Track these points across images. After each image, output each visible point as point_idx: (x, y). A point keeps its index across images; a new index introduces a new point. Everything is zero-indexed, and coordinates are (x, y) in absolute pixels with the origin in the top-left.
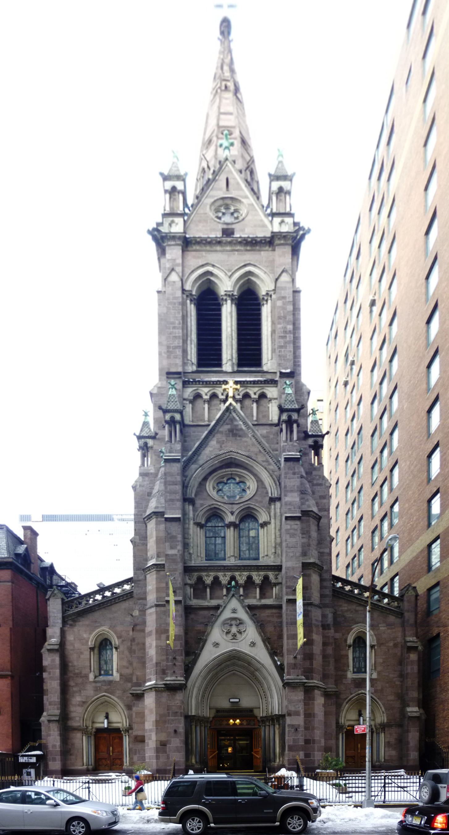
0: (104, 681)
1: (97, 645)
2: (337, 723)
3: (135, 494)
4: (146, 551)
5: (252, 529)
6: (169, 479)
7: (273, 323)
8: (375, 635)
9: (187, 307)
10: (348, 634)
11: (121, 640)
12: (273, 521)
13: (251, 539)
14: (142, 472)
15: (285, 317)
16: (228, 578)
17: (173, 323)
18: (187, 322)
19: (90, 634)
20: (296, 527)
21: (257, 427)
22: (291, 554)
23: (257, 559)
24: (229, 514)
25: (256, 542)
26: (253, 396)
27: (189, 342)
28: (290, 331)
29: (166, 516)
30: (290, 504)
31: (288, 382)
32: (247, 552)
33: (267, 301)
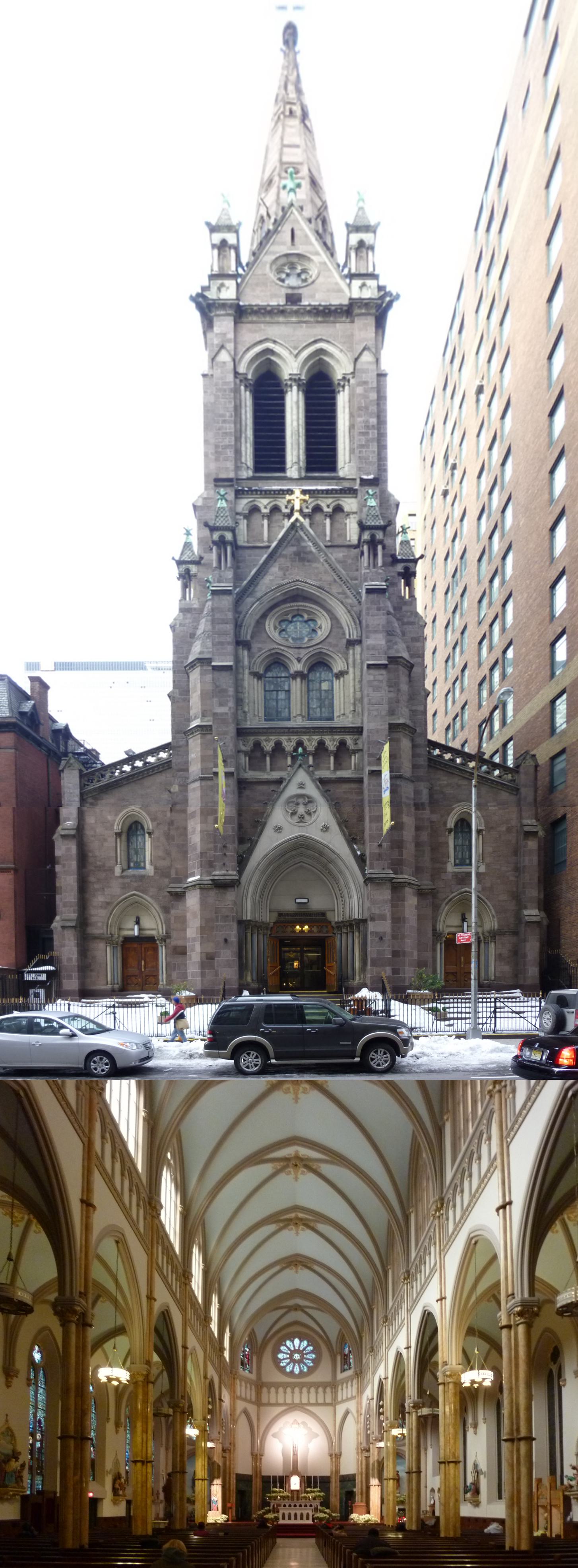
0: (134, 876)
1: (125, 829)
2: (434, 929)
3: (174, 636)
4: (188, 709)
5: (325, 681)
6: (218, 616)
7: (351, 415)
8: (483, 816)
9: (240, 395)
10: (448, 815)
11: (155, 823)
12: (351, 670)
13: (323, 693)
14: (183, 606)
15: (367, 408)
16: (293, 744)
17: (222, 416)
18: (241, 414)
19: (116, 815)
20: (380, 678)
21: (331, 550)
22: (375, 713)
23: (332, 719)
24: (295, 661)
25: (330, 697)
26: (326, 509)
27: (243, 440)
28: (373, 426)
29: (213, 664)
30: (374, 648)
31: (371, 492)
32: (318, 710)
33: (343, 387)
